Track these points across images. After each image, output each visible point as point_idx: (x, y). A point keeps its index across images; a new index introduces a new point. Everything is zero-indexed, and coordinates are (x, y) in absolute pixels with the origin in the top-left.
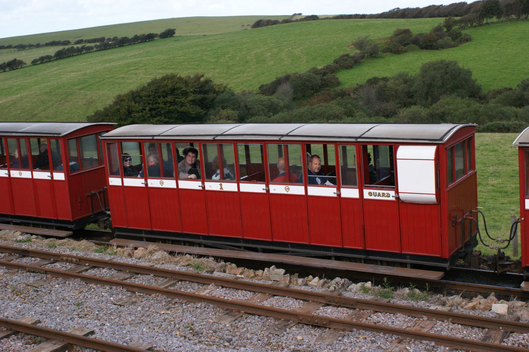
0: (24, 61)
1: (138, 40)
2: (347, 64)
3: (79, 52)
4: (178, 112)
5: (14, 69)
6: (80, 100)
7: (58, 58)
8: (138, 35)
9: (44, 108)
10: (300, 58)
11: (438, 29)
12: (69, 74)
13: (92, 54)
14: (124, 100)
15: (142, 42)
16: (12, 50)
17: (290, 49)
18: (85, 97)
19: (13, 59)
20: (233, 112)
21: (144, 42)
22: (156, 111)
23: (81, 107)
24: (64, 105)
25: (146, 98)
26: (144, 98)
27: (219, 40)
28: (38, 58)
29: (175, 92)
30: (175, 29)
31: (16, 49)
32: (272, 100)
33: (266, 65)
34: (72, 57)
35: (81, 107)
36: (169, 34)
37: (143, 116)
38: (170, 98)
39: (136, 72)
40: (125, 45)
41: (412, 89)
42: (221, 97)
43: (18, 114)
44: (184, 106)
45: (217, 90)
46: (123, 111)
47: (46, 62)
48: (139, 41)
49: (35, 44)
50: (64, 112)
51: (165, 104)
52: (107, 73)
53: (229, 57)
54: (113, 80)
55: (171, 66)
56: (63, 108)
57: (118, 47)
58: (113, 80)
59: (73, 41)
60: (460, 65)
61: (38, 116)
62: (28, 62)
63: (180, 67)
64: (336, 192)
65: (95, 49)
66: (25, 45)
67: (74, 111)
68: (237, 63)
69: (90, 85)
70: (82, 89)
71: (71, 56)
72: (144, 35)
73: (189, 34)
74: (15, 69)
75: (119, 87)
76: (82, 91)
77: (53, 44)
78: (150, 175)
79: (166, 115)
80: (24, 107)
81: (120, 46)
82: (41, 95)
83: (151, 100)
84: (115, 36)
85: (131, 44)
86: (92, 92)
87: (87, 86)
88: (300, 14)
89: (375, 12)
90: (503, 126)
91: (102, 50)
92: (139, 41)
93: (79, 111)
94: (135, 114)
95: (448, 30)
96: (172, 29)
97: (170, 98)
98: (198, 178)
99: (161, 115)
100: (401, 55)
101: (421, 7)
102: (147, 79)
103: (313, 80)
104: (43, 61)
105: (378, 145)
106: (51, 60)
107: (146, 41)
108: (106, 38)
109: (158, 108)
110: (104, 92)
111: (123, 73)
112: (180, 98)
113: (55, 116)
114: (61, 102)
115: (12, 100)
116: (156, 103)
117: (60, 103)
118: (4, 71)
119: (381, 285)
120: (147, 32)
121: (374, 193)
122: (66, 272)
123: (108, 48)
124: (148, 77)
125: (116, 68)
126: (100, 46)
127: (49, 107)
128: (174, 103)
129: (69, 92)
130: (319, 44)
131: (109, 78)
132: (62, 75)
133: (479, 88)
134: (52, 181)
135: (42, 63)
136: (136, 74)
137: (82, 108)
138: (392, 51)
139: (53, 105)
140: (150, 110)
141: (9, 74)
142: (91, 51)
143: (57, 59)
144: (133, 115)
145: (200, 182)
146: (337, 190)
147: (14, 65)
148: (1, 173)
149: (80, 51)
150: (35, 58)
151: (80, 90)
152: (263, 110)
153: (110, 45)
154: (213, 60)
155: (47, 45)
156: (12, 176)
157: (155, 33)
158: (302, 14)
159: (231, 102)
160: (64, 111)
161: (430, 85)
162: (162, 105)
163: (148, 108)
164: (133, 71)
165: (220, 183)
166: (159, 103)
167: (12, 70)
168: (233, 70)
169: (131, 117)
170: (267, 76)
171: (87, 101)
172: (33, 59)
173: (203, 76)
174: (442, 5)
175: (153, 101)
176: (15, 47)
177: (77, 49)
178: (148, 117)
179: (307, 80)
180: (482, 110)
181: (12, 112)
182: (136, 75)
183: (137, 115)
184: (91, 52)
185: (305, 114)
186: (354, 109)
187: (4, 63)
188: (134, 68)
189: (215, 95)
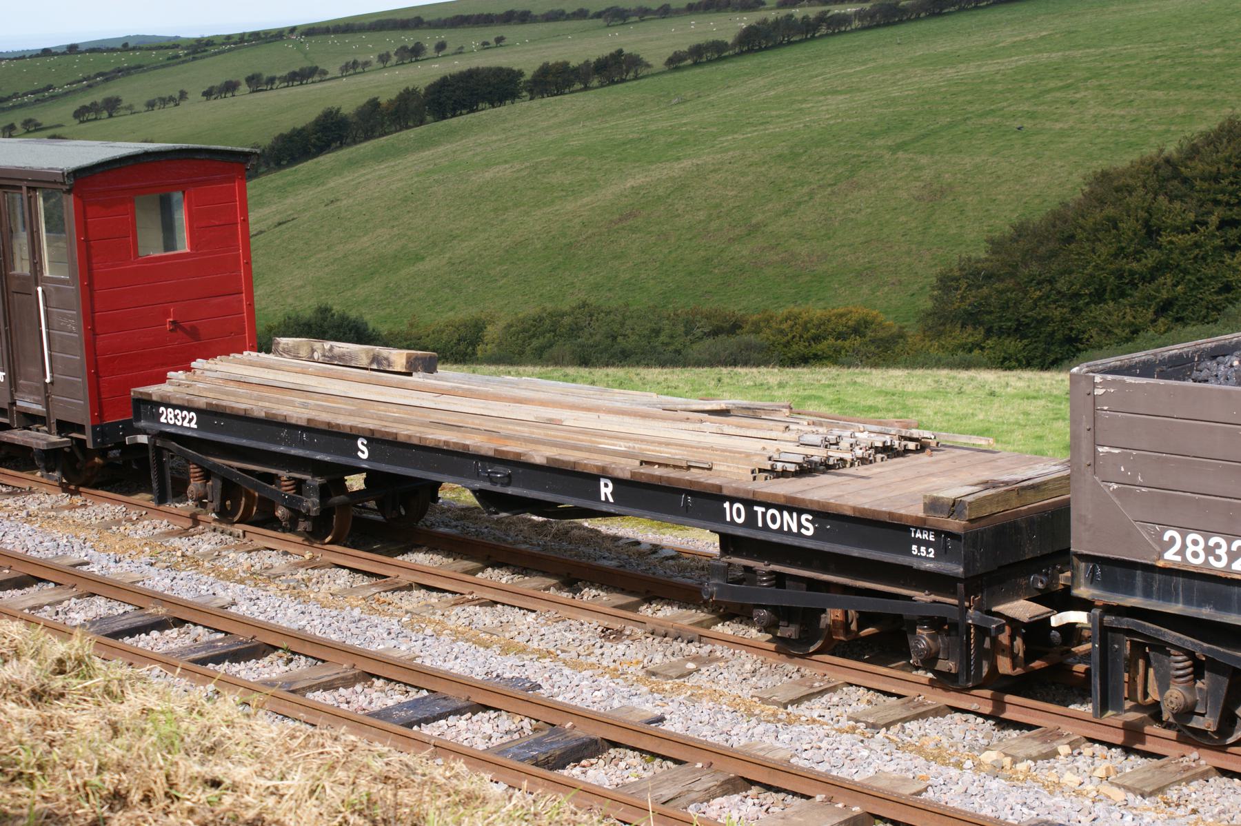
0: (645, 57)
5: (613, 82)
6: (900, 183)
9: (784, 206)
12: (822, 98)
13: (844, 38)
14: (1130, 190)
18: (916, 175)
19: (613, 50)
23: (910, 204)
24: (850, 198)
26: (1198, 184)
28: (685, 48)
31: (601, 22)
34: (787, 49)
35: (910, 204)
37: (1196, 245)
39: (1070, 95)
40: (946, 11)
43: (700, 222)
46: (1128, 225)
47: (710, 61)
49: (655, 7)
52: (969, 98)
55: (1191, 79)
57: (927, 17)
61: (770, 229)
62: (658, 62)
63: (1224, 83)
65: (856, 24)
66: (627, 8)
67: (888, 217)
69: (924, 136)
70: (901, 146)
71: (785, 45)
74: (617, 82)
75: (1026, 145)
76: (900, 154)
82: (764, 163)
83: (1223, 192)
85: (967, 10)
91: (878, 26)
93: (903, 219)
94: (1174, 239)
102: (1115, 119)
104: (700, 56)
105: (439, 484)
110: (978, 160)
111: (1027, 99)
113: (823, 232)
114: (836, 188)
115: (673, 179)
117: (833, 193)
118: (586, 88)
124: (1117, 112)
126: (871, 15)
127: (799, 204)
129: (859, 156)
136: (1072, 103)
137: (912, 209)
139: (811, 195)
140: (1224, 224)
142: (843, 29)
143: (741, 53)
144: (1163, 240)
150: (676, 49)
151: (895, 149)
160: (852, 216)
163: (1214, 220)
164: (1058, 94)
167: (608, 85)
169: (1159, 247)
171: (924, 187)
172: (669, 52)
176: (598, 15)
177: (802, 23)
178: (1215, 248)
181: (679, 216)
182: (1076, 106)
183: (1179, 239)
187: (587, 63)
188: (1061, 84)
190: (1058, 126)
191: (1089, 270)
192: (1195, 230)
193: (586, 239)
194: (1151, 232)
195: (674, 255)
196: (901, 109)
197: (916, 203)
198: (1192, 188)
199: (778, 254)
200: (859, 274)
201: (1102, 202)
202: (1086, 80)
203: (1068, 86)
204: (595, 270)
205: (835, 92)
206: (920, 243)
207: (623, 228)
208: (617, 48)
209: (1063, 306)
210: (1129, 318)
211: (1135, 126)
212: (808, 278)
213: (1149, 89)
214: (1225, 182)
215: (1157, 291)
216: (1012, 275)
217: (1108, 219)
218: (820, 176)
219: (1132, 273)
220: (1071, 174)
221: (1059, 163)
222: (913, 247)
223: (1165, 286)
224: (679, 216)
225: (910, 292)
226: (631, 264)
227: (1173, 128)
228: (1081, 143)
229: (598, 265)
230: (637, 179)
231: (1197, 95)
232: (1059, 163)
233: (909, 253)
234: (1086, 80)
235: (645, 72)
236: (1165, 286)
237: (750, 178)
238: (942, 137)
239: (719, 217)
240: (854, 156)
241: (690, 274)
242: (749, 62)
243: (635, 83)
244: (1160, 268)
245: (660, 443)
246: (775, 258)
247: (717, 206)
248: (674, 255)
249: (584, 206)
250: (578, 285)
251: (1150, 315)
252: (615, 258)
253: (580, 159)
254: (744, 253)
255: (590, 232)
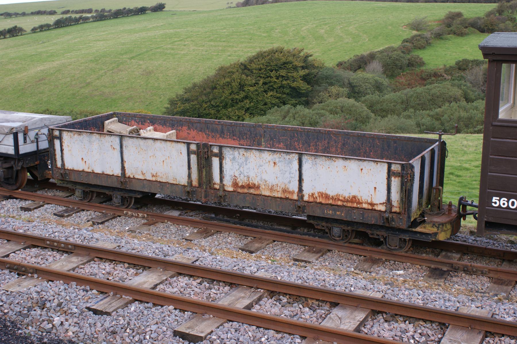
0: (24, 28)
1: (131, 12)
2: (420, 44)
3: (76, 22)
4: (290, 87)
5: (14, 36)
7: (57, 26)
8: (131, 8)
11: (489, 14)
14: (233, 73)
15: (135, 15)
19: (14, 26)
25: (257, 72)
30: (165, 4)
34: (70, 27)
35: (140, 77)
37: (256, 91)
46: (235, 84)
47: (45, 30)
48: (132, 14)
49: (20, 13)
51: (278, 79)
52: (150, 43)
58: (162, 50)
59: (59, 11)
61: (93, 84)
65: (91, 20)
68: (292, 38)
69: (139, 55)
72: (136, 8)
74: (15, 36)
75: (174, 58)
76: (132, 60)
80: (73, 75)
81: (114, 18)
82: (86, 63)
83: (262, 74)
84: (103, 8)
87: (137, 56)
91: (98, 21)
92: (132, 14)
93: (138, 81)
96: (163, 3)
97: (283, 73)
99: (272, 90)
100: (466, 37)
103: (402, 59)
104: (42, 28)
106: (50, 28)
107: (138, 14)
108: (94, 9)
109: (270, 82)
110: (159, 63)
112: (291, 73)
113: (112, 85)
114: (113, 71)
116: (268, 77)
117: (113, 72)
118: (5, 38)
124: (200, 48)
127: (102, 76)
135: (41, 31)
136: (185, 45)
138: (455, 34)
139: (105, 73)
140: (265, 84)
141: (10, 41)
143: (55, 28)
147: (14, 32)
149: (77, 21)
153: (106, 16)
154: (264, 35)
157: (147, 6)
160: (121, 80)
162: (274, 79)
163: (261, 82)
164: (179, 43)
166: (271, 77)
171: (143, 71)
172: (32, 27)
175: (265, 74)
181: (60, 79)
182: (186, 46)
183: (252, 89)
186: (468, 91)
187: (5, 30)
190: (183, 52)
191: (223, 98)
192: (255, 86)
193: (28, 87)
194: (241, 87)
195: (61, 92)
196: (129, 46)
197: (142, 76)
198: (252, 72)
199: (98, 92)
200: (128, 99)
201: (224, 77)
202: (187, 38)
203: (181, 40)
204: (34, 97)
205: (99, 41)
206: (146, 89)
207: (41, 84)
208: (15, 25)
209: (214, 110)
210: (237, 113)
211: (207, 53)
212: (110, 100)
213: (208, 41)
214: (262, 71)
215: (245, 105)
216: (197, 99)
217: (227, 82)
218: (107, 67)
219: (237, 99)
220: (191, 67)
221: (187, 64)
222: (144, 90)
223: (247, 103)
224: (60, 79)
225: (146, 105)
226: (46, 95)
227: (220, 54)
228: (192, 58)
229: (34, 96)
230: (42, 68)
231: (225, 44)
232: (187, 64)
233: (143, 92)
234: (187, 38)
235: (24, 33)
236: (247, 103)
237: (82, 68)
238: (145, 55)
239: (75, 80)
240: (117, 61)
241: (69, 99)
242: (61, 31)
243: (21, 36)
244: (246, 97)
245: (179, 142)
246: (98, 93)
247: (73, 76)
248: (61, 92)
249: (25, 76)
250: (29, 102)
251: (243, 113)
252: (40, 93)
253: (17, 60)
254: (87, 92)
255: (29, 85)
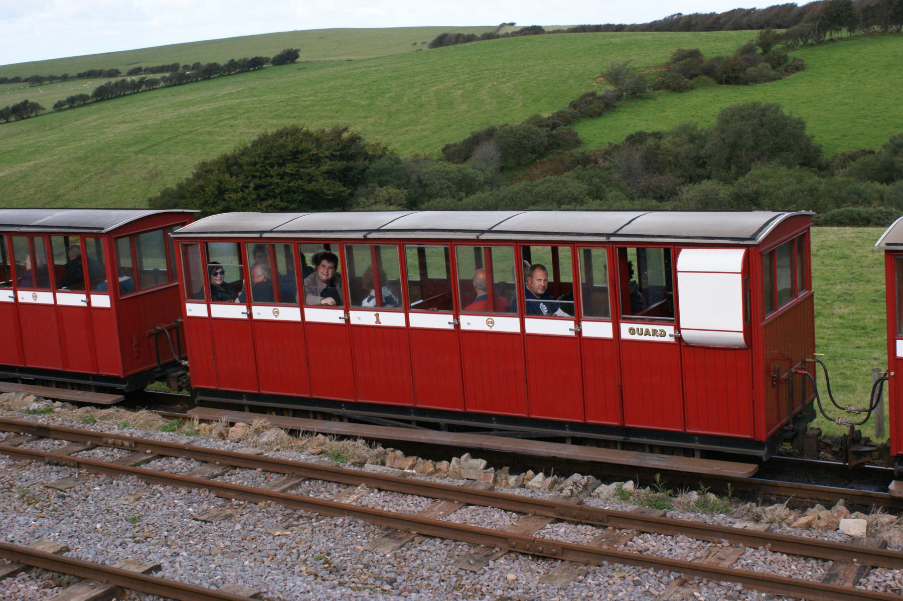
0: (41, 104)
1: (235, 68)
2: (592, 109)
3: (135, 89)
4: (304, 191)
5: (23, 119)
6: (137, 171)
7: (99, 98)
8: (236, 60)
9: (75, 185)
10: (512, 99)
11: (748, 50)
12: (118, 126)
13: (156, 91)
14: (211, 171)
15: (242, 72)
16: (21, 85)
17: (495, 83)
18: (145, 166)
19: (22, 101)
20: (397, 191)
21: (246, 71)
22: (266, 190)
23: (139, 182)
24: (110, 179)
25: (249, 168)
26: (245, 167)
27: (374, 69)
28: (65, 99)
29: (298, 158)
30: (298, 50)
31: (27, 84)
32: (464, 171)
33: (454, 111)
34: (123, 98)
35: (139, 182)
36: (288, 58)
37: (243, 198)
38: (289, 168)
39: (232, 122)
40: (213, 76)
41: (702, 152)
42: (377, 165)
43: (31, 194)
44: (315, 181)
45: (370, 153)
46: (209, 189)
47: (79, 106)
48: (237, 70)
49: (59, 75)
50: (109, 191)
51: (282, 178)
52: (183, 124)
53: (390, 97)
54: (192, 136)
55: (292, 113)
56: (108, 184)
57: (202, 80)
58: (192, 136)
59: (124, 69)
60: (786, 112)
61: (66, 197)
62: (49, 106)
63: (307, 115)
64: (573, 327)
65: (162, 84)
66: (43, 76)
67: (127, 189)
68: (404, 108)
69: (154, 145)
70: (140, 151)
71: (122, 96)
72: (245, 60)
73: (322, 59)
74: (26, 118)
75: (203, 149)
76: (140, 155)
77: (91, 74)
78: (256, 300)
79: (284, 196)
80: (42, 183)
81: (205, 79)
82: (70, 162)
83: (257, 171)
84: (197, 61)
85: (224, 76)
86: (158, 157)
87: (149, 147)
88: (512, 24)
89: (639, 21)
90: (859, 214)
91: (175, 85)
92: (237, 70)
93: (134, 190)
94: (231, 195)
95: (765, 52)
96: (294, 49)
97: (289, 168)
98: (338, 305)
99: (275, 197)
100: (685, 94)
101: (719, 11)
102: (250, 135)
103: (534, 137)
104: (74, 104)
106: (87, 102)
107: (249, 71)
108: (181, 65)
109: (270, 184)
110: (178, 157)
111: (211, 125)
112: (307, 168)
113: (93, 198)
114: (103, 174)
115: (21, 171)
116: (267, 176)
117: (102, 176)
118: (8, 122)
119: (650, 487)
120: (250, 55)
121: (638, 329)
122: (113, 465)
123: (185, 81)
124: (252, 131)
125: (198, 116)
126: (170, 79)
127: (83, 183)
128: (297, 177)
129: (118, 157)
130: (545, 74)
131: (186, 134)
132: (106, 128)
133: (818, 151)
134: (89, 309)
135: (71, 107)
136: (232, 126)
137: (140, 184)
138: (668, 88)
139: (90, 179)
140: (257, 188)
141: (15, 126)
142: (155, 87)
143: (97, 101)
144: (226, 196)
145: (342, 312)
146: (575, 325)
147: (23, 111)
148: (2, 295)
149: (136, 88)
150: (59, 99)
151: (136, 153)
152: (449, 187)
153: (189, 77)
154: (363, 103)
155: (81, 76)
156: (20, 300)
157: (264, 56)
158: (515, 24)
159: (394, 174)
160: (109, 189)
161: (734, 146)
162: (276, 180)
163: (252, 185)
164: (226, 122)
165: (375, 313)
166: (272, 176)
167: (21, 120)
168: (398, 120)
169: (224, 200)
170: (455, 129)
171: (148, 173)
172: (55, 101)
173: (346, 130)
174: (755, 8)
175: (262, 172)
176: (26, 80)
177: (131, 84)
178: (253, 200)
179: (524, 137)
180: (822, 187)
181: (20, 192)
182: (233, 128)
183: (234, 196)
184: (156, 89)
185: (521, 194)
186: (604, 186)
187: (7, 108)
188: (229, 116)
189: (367, 162)
